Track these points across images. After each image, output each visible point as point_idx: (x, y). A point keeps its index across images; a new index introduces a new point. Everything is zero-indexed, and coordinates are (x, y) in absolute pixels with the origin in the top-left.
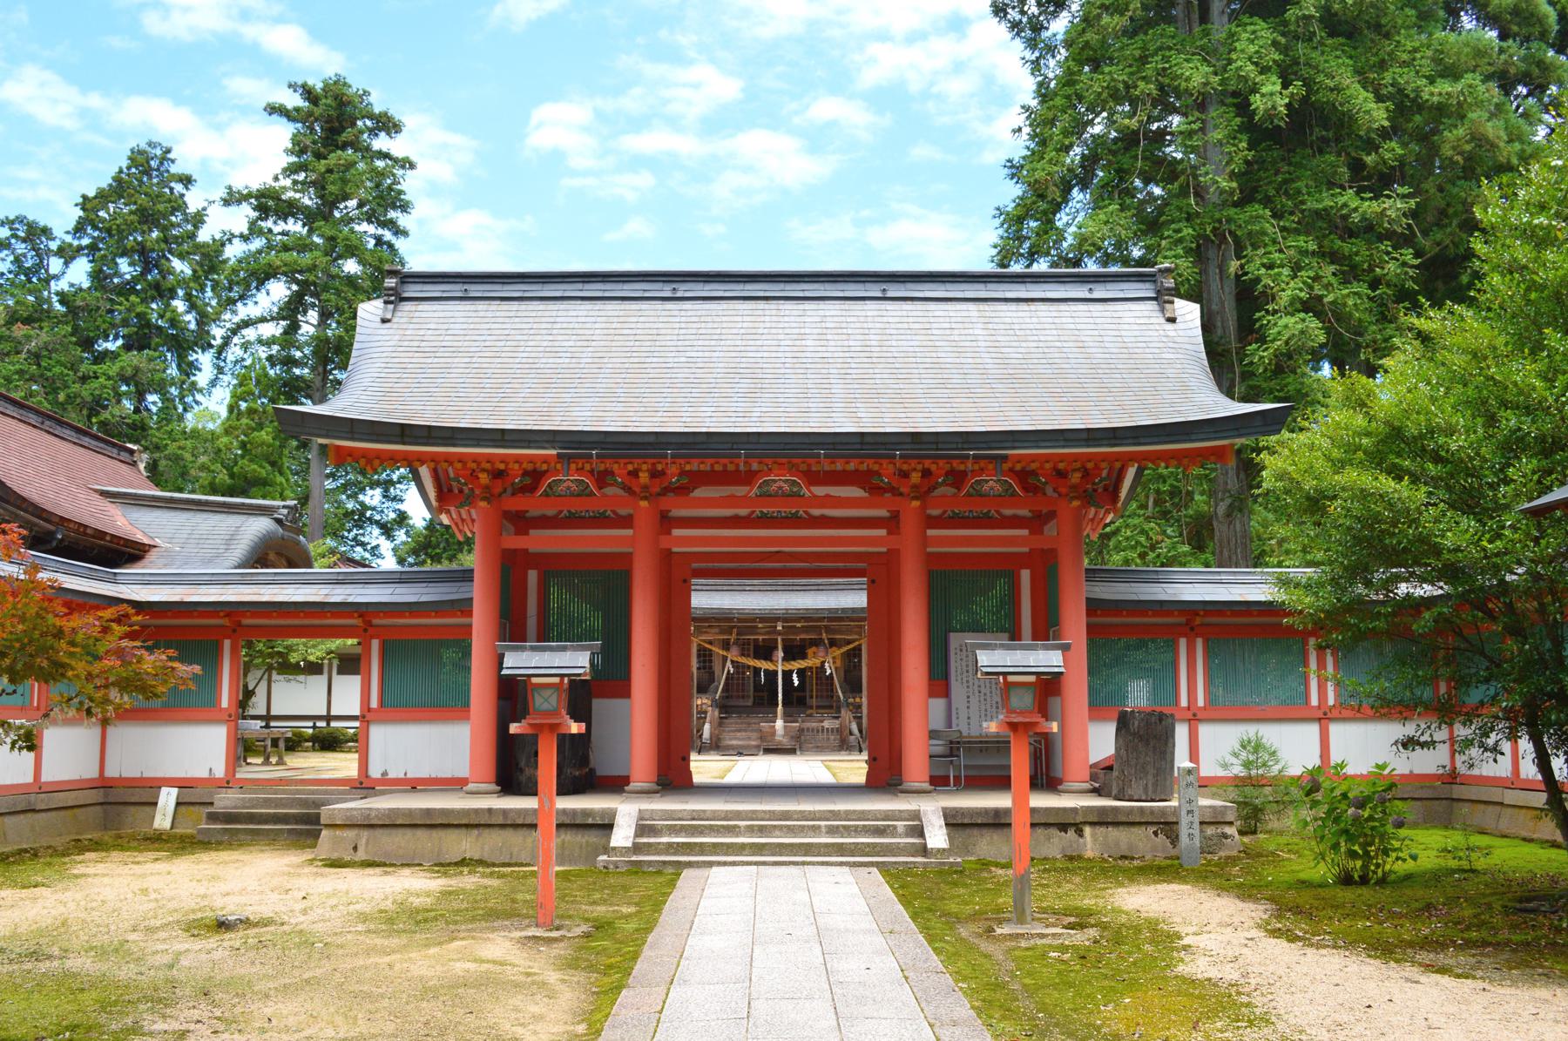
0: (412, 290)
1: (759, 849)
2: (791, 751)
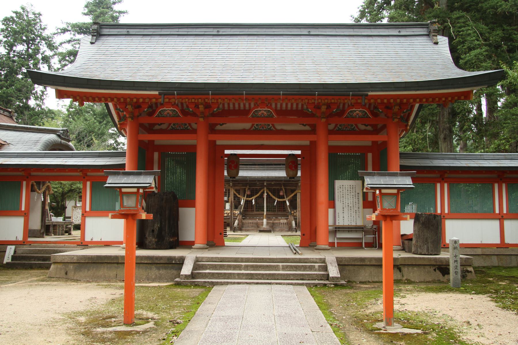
0: (105, 31)
1: (251, 276)
2: (269, 231)
